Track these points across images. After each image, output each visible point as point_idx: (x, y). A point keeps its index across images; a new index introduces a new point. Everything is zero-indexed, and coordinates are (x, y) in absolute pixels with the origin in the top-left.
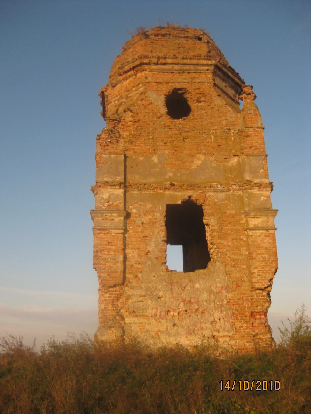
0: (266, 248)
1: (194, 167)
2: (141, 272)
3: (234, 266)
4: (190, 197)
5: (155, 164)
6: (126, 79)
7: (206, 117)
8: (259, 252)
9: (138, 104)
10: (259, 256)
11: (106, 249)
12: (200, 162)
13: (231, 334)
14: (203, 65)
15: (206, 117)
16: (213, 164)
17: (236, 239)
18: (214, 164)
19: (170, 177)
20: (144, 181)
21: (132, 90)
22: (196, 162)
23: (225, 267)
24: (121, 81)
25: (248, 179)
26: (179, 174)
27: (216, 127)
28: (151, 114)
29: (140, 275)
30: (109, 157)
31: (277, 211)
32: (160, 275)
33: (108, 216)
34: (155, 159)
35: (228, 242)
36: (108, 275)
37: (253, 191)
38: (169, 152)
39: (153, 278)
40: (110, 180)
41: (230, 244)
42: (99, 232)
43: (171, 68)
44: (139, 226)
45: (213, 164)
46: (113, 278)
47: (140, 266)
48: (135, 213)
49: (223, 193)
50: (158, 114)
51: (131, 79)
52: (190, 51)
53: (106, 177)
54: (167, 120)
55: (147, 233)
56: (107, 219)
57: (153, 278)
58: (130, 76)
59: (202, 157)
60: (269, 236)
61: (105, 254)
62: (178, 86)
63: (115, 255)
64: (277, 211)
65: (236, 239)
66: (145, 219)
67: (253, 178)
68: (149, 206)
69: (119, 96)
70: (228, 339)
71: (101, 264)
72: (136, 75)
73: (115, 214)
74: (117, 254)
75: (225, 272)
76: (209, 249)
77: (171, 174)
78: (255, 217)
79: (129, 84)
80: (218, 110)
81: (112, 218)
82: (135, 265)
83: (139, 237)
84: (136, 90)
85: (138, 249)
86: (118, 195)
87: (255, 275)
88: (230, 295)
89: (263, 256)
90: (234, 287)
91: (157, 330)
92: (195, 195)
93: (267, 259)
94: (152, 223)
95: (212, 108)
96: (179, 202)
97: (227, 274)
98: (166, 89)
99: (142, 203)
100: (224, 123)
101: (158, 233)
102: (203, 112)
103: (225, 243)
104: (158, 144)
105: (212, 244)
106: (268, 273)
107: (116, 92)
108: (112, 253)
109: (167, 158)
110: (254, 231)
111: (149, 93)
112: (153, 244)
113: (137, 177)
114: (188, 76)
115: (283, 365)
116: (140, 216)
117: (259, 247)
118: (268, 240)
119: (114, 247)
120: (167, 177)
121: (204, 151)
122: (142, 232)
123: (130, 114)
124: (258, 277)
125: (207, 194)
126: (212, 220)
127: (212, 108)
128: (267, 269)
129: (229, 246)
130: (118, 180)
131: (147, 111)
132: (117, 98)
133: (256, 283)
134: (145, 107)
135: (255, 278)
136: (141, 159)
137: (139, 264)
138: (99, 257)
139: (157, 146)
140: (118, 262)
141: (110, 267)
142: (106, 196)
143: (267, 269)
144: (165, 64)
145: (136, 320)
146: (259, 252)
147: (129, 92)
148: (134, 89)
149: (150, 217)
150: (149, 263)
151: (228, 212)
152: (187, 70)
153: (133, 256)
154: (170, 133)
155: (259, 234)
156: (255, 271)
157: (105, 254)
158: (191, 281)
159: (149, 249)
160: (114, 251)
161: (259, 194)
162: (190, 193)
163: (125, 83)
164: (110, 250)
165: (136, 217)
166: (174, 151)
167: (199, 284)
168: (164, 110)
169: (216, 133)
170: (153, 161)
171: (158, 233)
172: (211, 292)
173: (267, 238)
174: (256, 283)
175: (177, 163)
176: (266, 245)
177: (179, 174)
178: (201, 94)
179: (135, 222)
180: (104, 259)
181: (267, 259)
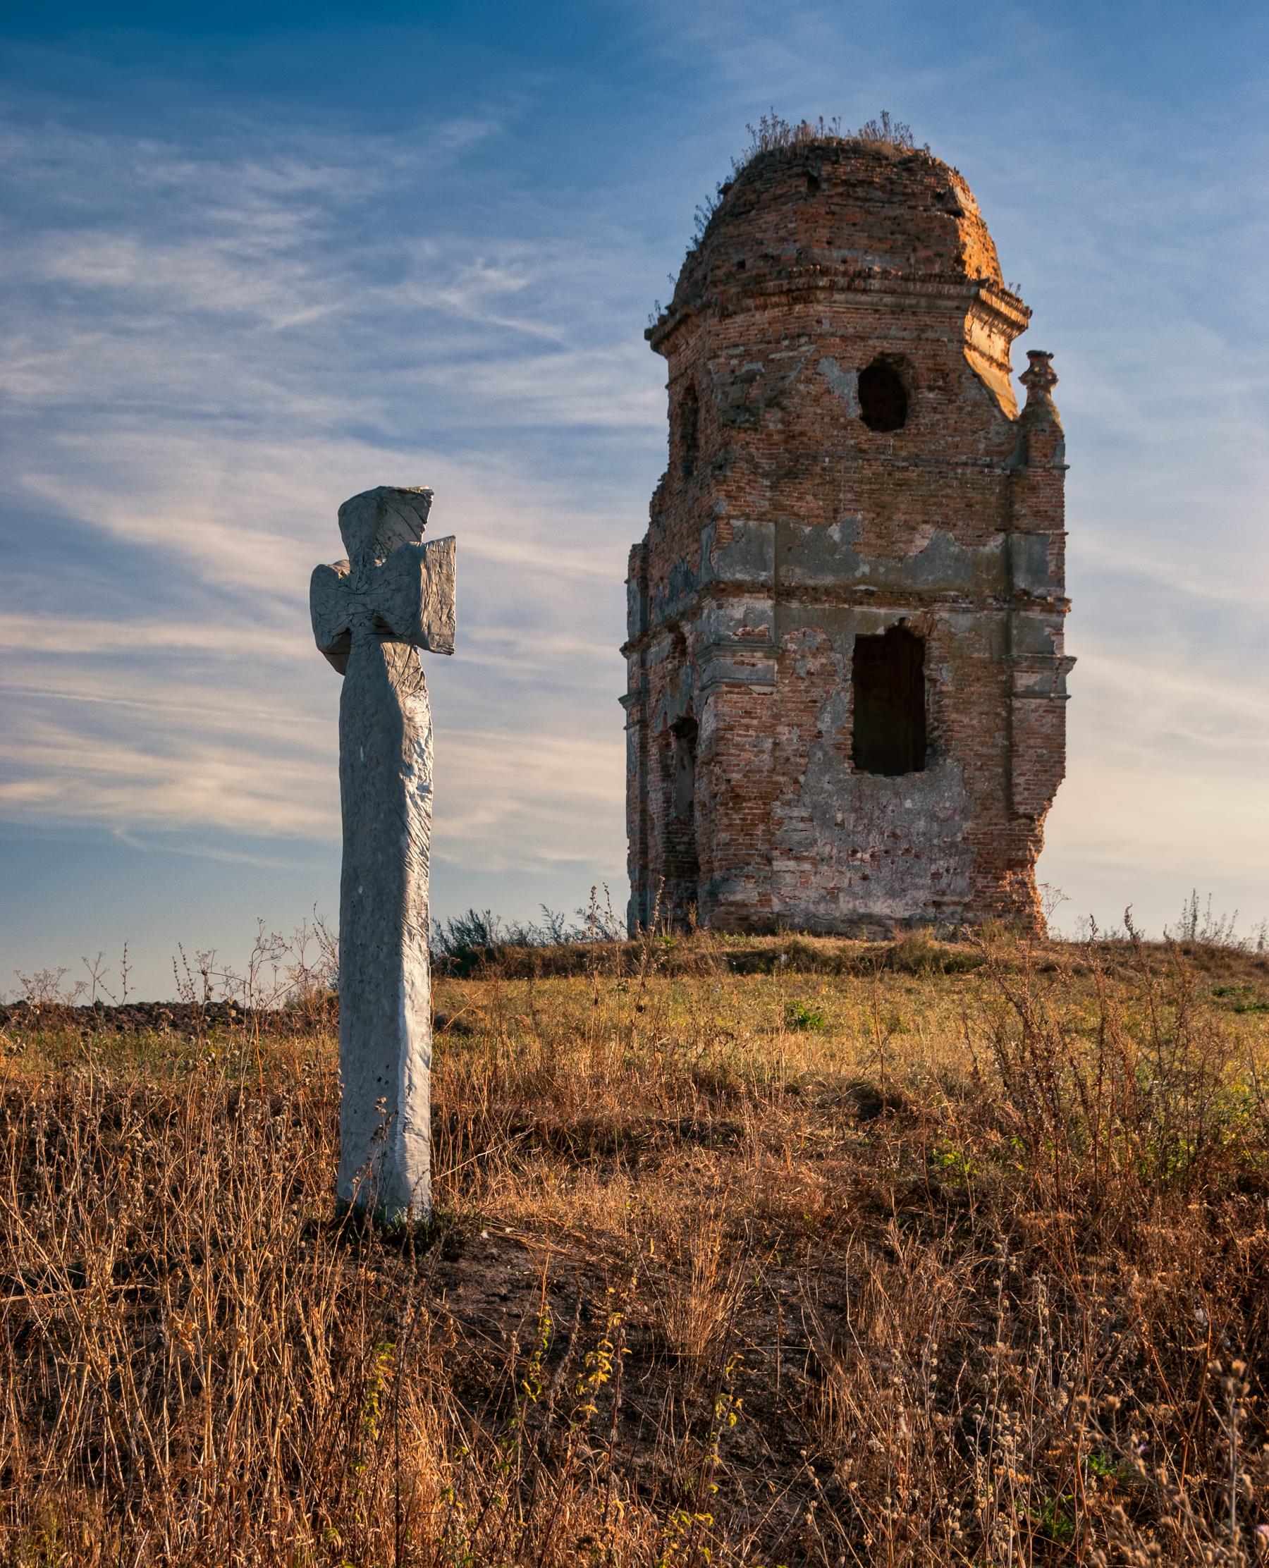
0: (1047, 737)
1: (913, 553)
2: (804, 773)
3: (981, 769)
4: (902, 620)
5: (835, 542)
6: (764, 307)
7: (944, 432)
8: (1031, 742)
9: (798, 391)
10: (1031, 752)
11: (741, 725)
12: (926, 543)
13: (967, 899)
14: (949, 297)
15: (944, 432)
16: (952, 549)
17: (987, 714)
18: (954, 550)
19: (864, 574)
20: (811, 582)
21: (778, 342)
22: (918, 543)
23: (964, 769)
24: (749, 310)
25: (1023, 586)
26: (882, 570)
27: (964, 457)
28: (827, 420)
29: (802, 779)
30: (745, 526)
31: (1073, 660)
32: (840, 781)
33: (747, 657)
34: (835, 532)
35: (971, 719)
36: (745, 776)
37: (1031, 615)
38: (864, 519)
39: (826, 786)
40: (747, 578)
41: (974, 722)
42: (726, 689)
43: (875, 299)
44: (803, 679)
45: (952, 549)
46: (754, 782)
47: (802, 761)
48: (795, 652)
49: (969, 615)
50: (842, 420)
51: (776, 312)
52: (917, 244)
53: (740, 572)
54: (865, 437)
55: (816, 693)
56: (743, 663)
57: (826, 786)
58: (777, 305)
59: (929, 529)
60: (1054, 712)
61: (739, 735)
62: (886, 346)
63: (758, 737)
64: (1073, 660)
65: (987, 714)
66: (813, 664)
67: (1033, 583)
68: (821, 637)
69: (742, 348)
70: (959, 909)
71: (732, 755)
72: (790, 305)
73: (759, 655)
74: (762, 734)
75: (963, 779)
76: (928, 729)
77: (865, 569)
78: (1030, 669)
79: (770, 323)
80: (970, 414)
81: (753, 661)
82: (792, 759)
83: (802, 702)
84: (788, 348)
85: (799, 726)
86: (763, 612)
87: (1021, 789)
88: (968, 825)
89: (1039, 751)
90: (979, 808)
91: (832, 885)
92: (912, 615)
93: (1045, 758)
94: (827, 673)
95: (960, 409)
96: (881, 631)
97: (966, 783)
98: (861, 356)
99: (809, 631)
100: (982, 446)
101: (838, 694)
102: (938, 416)
103: (966, 721)
104: (841, 496)
105: (936, 719)
106: (1045, 785)
107: (733, 333)
108: (751, 732)
109: (860, 530)
110: (1025, 701)
111: (825, 365)
112: (827, 717)
113: (798, 571)
114: (912, 321)
115: (998, 991)
116: (803, 657)
117: (1031, 733)
118: (1050, 719)
119: (755, 722)
120: (858, 574)
121: (938, 518)
122: (807, 692)
123: (779, 415)
124: (1026, 793)
125: (937, 617)
126: (944, 673)
127: (960, 409)
128: (1044, 778)
129: (973, 727)
130: (762, 578)
131: (819, 411)
132: (736, 352)
133: (1020, 804)
134: (816, 400)
135: (1020, 794)
136: (808, 530)
137: (801, 756)
138: (728, 740)
139: (840, 501)
140: (763, 752)
141: (749, 763)
142: (738, 613)
143: (1044, 778)
144: (865, 291)
145: (792, 864)
146: (1031, 742)
147: (772, 346)
148: (786, 343)
149: (823, 661)
150: (820, 754)
151: (975, 655)
152: (911, 306)
153: (790, 740)
154: (867, 472)
155: (1033, 706)
156: (1021, 780)
157: (739, 735)
158: (897, 794)
159: (822, 726)
160: (757, 729)
161: (1041, 621)
162: (902, 612)
163: (761, 318)
164: (747, 727)
165: (796, 660)
166: (874, 515)
167: (913, 800)
168: (855, 411)
169: (963, 474)
170: (831, 537)
171: (838, 694)
172: (932, 817)
173: (1051, 716)
174: (1020, 804)
175: (880, 542)
176: (1046, 730)
177: (882, 570)
178: (937, 370)
179: (794, 669)
180: (737, 745)
181: (1045, 758)
